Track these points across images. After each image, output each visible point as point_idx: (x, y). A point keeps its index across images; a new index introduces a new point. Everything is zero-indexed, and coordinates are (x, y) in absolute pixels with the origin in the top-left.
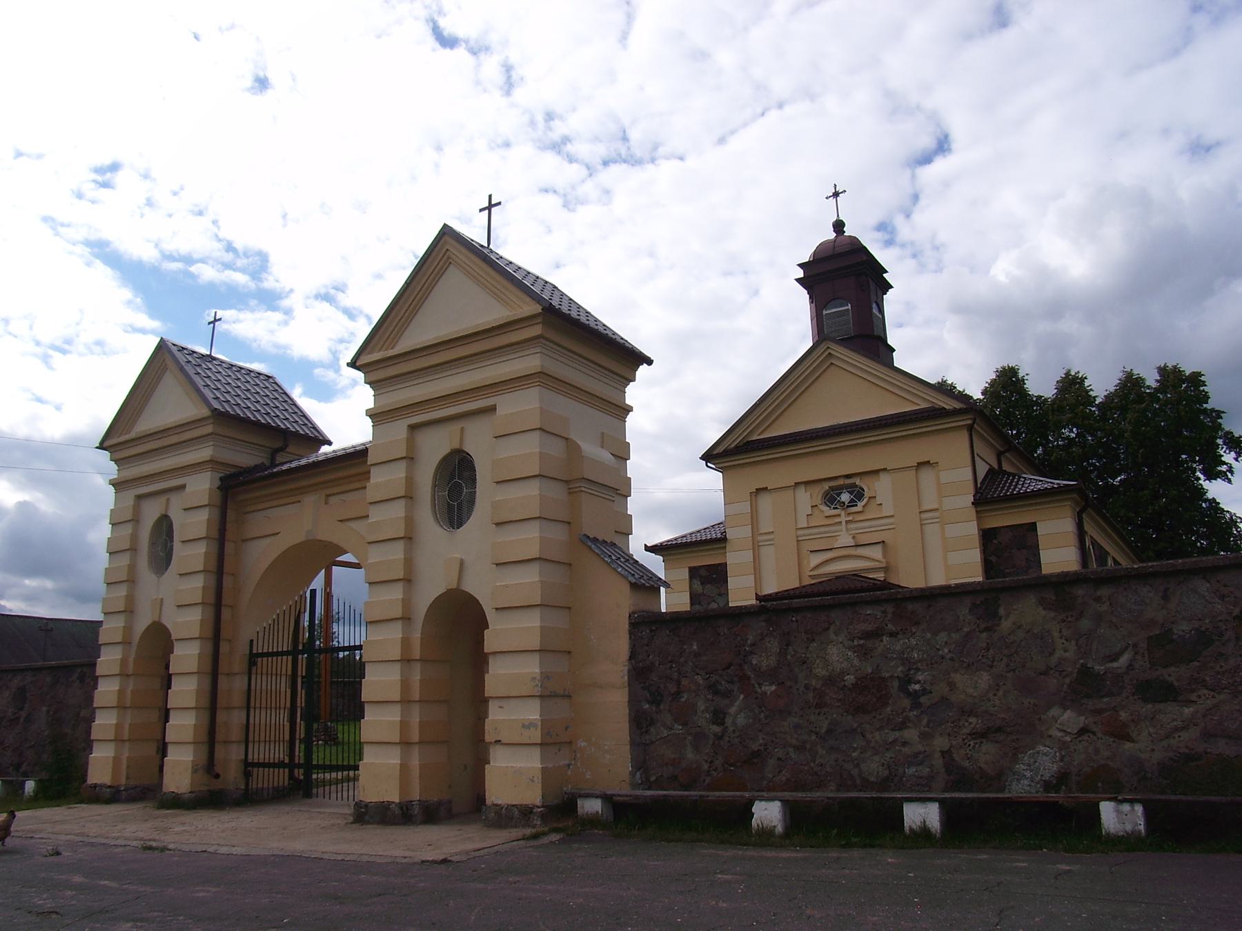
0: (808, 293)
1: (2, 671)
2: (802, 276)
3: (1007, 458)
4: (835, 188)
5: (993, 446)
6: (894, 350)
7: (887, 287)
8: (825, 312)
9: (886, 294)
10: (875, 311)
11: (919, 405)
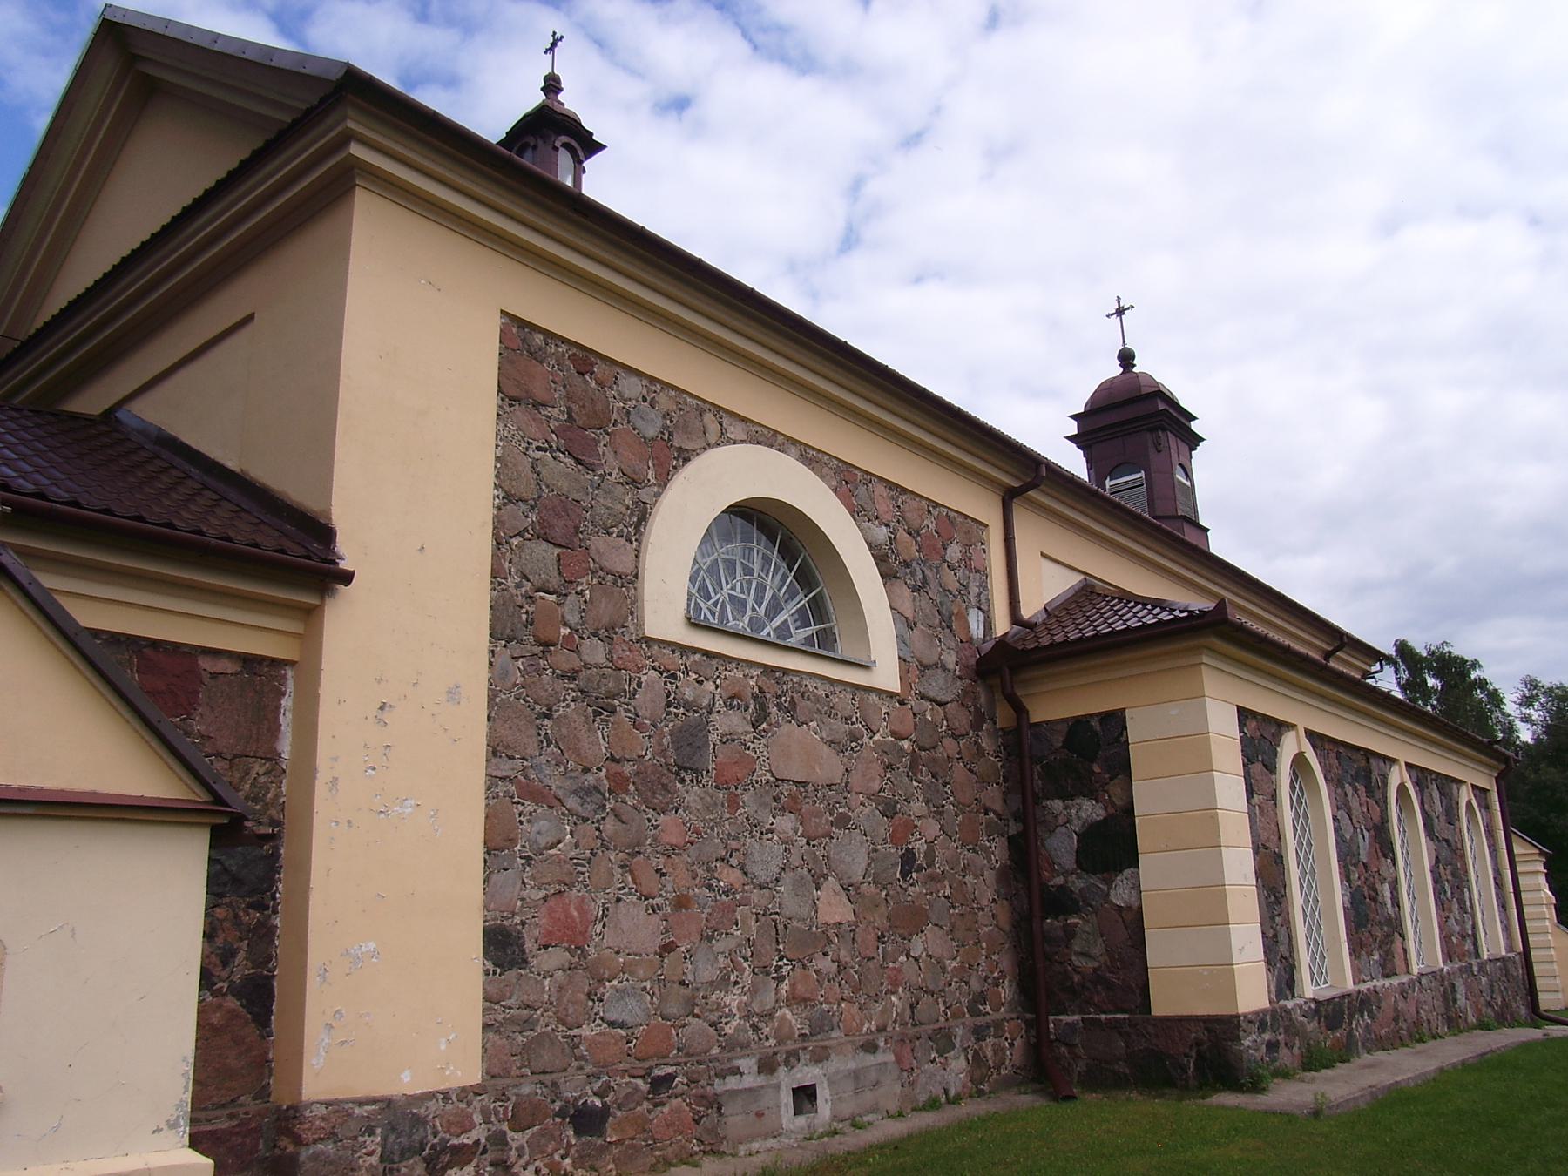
2: (1076, 432)
4: (1119, 302)
6: (1207, 530)
8: (1108, 483)
10: (1180, 477)
11: (200, 797)
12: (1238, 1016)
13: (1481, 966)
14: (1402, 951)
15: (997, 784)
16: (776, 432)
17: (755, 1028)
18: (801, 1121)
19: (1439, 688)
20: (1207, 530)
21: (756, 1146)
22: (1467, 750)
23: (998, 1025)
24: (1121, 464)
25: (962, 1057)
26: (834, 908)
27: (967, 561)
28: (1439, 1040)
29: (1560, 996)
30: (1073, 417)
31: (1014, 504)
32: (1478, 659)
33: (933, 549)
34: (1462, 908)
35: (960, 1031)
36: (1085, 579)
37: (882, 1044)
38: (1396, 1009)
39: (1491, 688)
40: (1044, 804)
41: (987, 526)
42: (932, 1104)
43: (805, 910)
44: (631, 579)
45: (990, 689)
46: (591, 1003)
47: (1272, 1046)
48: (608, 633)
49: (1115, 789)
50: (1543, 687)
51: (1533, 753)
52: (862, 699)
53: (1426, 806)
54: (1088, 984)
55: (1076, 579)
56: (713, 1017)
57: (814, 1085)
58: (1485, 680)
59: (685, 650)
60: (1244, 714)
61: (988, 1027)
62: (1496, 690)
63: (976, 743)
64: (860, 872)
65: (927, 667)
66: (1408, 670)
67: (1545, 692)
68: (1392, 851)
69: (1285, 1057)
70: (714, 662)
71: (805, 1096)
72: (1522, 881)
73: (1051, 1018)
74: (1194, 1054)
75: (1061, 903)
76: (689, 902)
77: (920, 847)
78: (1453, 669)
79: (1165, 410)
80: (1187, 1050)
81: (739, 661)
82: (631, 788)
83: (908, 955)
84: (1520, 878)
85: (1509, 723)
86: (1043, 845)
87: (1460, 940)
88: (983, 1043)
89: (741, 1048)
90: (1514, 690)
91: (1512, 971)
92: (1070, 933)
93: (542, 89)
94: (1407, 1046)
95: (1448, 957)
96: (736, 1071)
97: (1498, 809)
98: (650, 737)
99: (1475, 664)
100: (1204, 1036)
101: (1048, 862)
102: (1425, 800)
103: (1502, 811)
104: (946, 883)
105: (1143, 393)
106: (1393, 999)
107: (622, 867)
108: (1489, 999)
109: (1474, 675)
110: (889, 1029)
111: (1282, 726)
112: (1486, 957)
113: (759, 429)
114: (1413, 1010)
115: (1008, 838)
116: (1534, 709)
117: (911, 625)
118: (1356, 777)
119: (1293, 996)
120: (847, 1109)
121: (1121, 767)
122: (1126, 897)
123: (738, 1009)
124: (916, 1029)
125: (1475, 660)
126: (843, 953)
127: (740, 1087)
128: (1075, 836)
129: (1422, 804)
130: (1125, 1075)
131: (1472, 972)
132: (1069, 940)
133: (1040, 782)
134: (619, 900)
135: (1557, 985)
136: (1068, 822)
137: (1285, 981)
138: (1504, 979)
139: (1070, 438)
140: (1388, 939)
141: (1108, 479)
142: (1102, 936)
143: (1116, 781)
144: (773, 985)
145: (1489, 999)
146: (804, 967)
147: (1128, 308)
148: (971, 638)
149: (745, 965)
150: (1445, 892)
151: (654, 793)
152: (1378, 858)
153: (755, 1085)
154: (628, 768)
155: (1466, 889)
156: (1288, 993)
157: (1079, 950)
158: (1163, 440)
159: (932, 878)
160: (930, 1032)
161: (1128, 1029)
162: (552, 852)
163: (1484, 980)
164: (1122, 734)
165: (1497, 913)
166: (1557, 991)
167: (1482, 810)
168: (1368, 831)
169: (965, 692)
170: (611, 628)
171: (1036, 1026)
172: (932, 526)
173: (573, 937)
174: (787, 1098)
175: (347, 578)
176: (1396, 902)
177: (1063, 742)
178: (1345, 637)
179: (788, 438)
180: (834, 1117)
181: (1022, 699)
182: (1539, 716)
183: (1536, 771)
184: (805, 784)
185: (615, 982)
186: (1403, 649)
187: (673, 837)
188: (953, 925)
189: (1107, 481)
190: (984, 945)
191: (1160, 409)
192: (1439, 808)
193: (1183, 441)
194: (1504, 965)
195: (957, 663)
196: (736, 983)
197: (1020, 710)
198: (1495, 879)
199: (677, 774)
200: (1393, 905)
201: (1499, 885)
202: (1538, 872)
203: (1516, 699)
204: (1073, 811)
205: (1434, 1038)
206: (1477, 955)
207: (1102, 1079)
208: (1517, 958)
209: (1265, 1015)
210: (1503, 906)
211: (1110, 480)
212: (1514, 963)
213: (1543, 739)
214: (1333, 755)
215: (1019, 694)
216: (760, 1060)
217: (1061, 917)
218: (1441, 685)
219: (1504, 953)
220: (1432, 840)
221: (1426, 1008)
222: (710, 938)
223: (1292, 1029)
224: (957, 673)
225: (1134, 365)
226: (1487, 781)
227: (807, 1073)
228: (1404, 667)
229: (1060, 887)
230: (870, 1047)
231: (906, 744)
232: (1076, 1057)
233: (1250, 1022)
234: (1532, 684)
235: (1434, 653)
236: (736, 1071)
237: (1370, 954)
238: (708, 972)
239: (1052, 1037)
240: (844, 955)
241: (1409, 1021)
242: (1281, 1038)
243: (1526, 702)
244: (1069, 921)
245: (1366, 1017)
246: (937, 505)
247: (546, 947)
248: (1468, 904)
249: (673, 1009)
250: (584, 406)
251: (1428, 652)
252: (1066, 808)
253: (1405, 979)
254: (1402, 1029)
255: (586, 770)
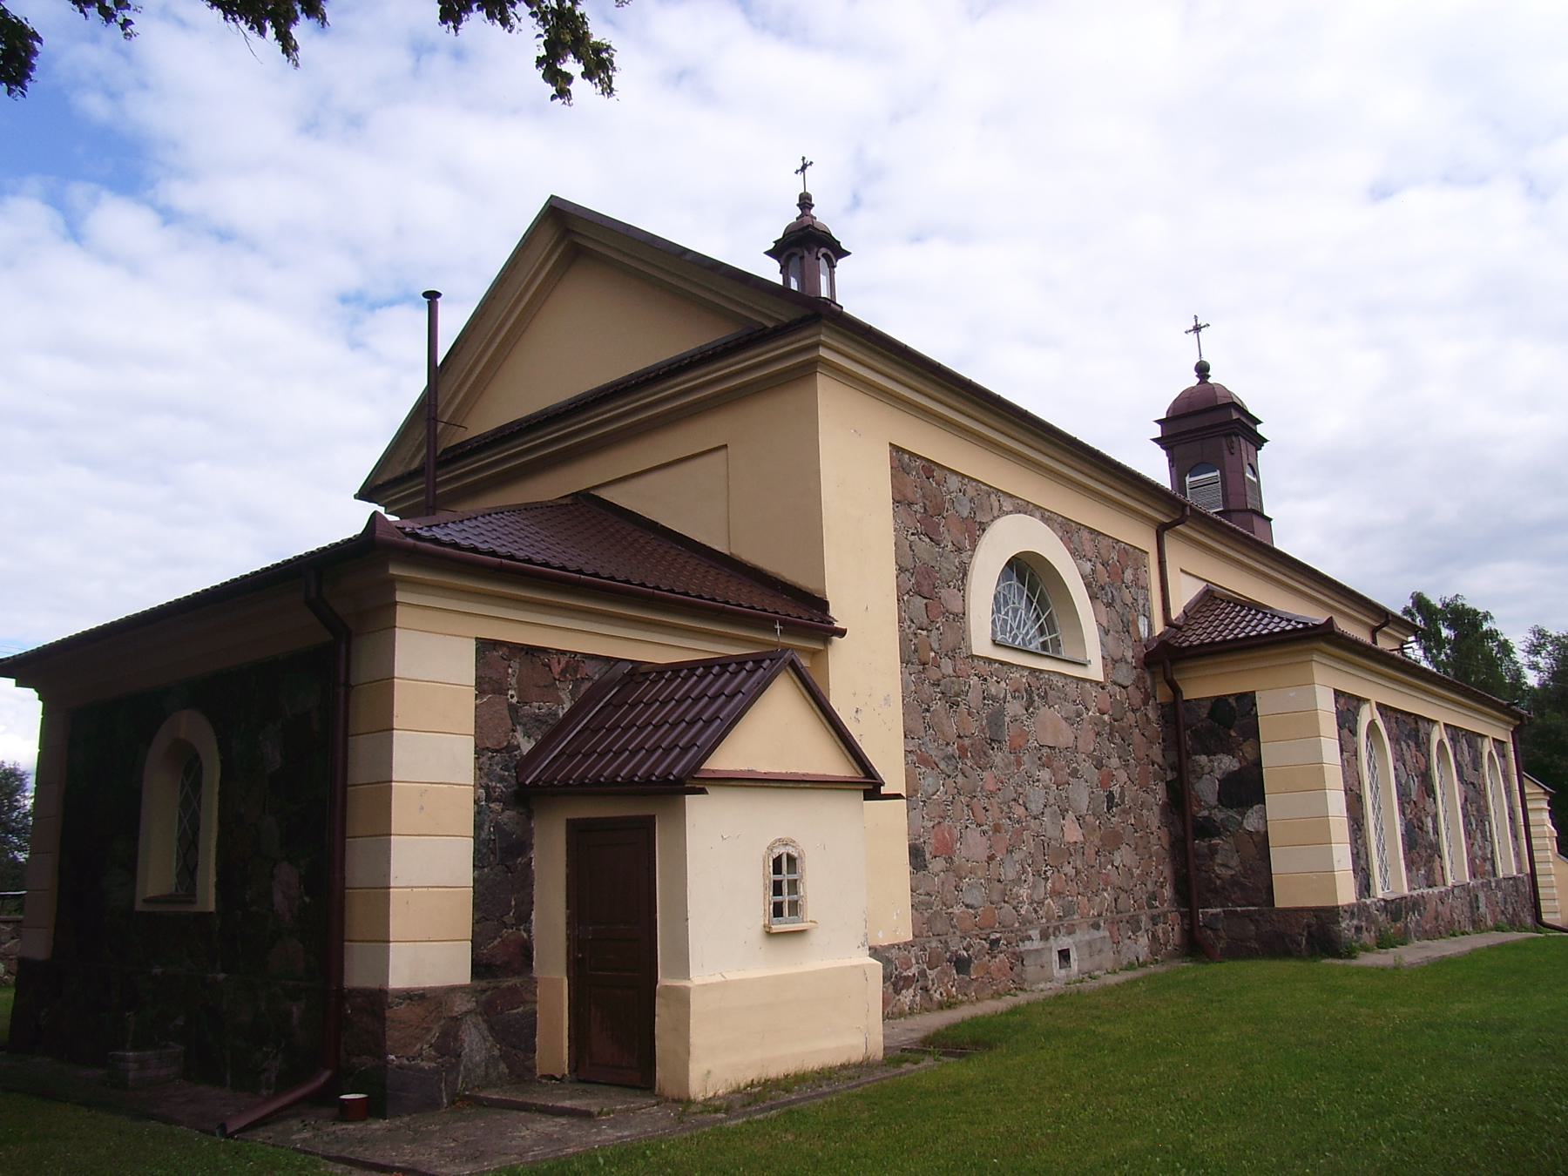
0: (1167, 455)
1: (2, 922)
2: (1160, 435)
3: (1387, 634)
4: (1196, 321)
5: (1365, 624)
7: (1259, 441)
8: (1188, 479)
9: (1260, 449)
10: (1249, 475)
12: (1338, 907)
13: (1498, 883)
14: (1439, 868)
15: (1159, 743)
16: (1028, 502)
17: (1036, 912)
18: (1063, 972)
19: (1453, 638)
20: (1270, 520)
21: (1041, 986)
22: (1488, 710)
23: (1165, 915)
24: (1197, 465)
25: (1146, 936)
26: (1073, 834)
27: (1136, 580)
28: (1467, 936)
29: (1559, 916)
30: (1158, 422)
31: (1165, 535)
32: (1489, 611)
33: (1116, 574)
34: (1484, 837)
35: (1144, 918)
36: (1207, 585)
37: (1102, 924)
38: (1437, 911)
39: (1502, 638)
40: (1193, 758)
41: (1147, 553)
42: (1130, 967)
43: (1057, 834)
44: (962, 616)
45: (1153, 675)
46: (956, 893)
47: (1358, 929)
48: (952, 654)
49: (1247, 748)
50: (1550, 636)
51: (1539, 698)
52: (1082, 688)
53: (1458, 756)
54: (1227, 887)
55: (1201, 586)
56: (1015, 903)
57: (1068, 950)
58: (1496, 631)
59: (990, 661)
60: (1338, 694)
61: (1159, 916)
62: (1507, 641)
63: (1146, 714)
64: (1086, 808)
65: (1116, 662)
66: (1424, 620)
67: (1553, 641)
68: (1434, 792)
69: (1368, 938)
70: (1005, 668)
71: (1064, 955)
72: (1531, 816)
73: (1200, 910)
74: (1305, 933)
75: (1207, 829)
76: (1000, 828)
77: (1116, 789)
78: (1466, 621)
79: (1238, 419)
80: (1301, 931)
81: (1018, 666)
82: (969, 755)
83: (1113, 865)
84: (1530, 814)
85: (1518, 670)
86: (1194, 789)
87: (1482, 863)
88: (1157, 927)
89: (1030, 923)
90: (1524, 639)
91: (1521, 887)
92: (1213, 851)
93: (798, 205)
94: (1444, 938)
95: (1473, 875)
96: (1030, 938)
97: (1513, 757)
98: (976, 721)
99: (1487, 616)
100: (1314, 921)
101: (1196, 800)
102: (1458, 752)
103: (1516, 759)
104: (1132, 815)
105: (1219, 403)
106: (1434, 903)
107: (967, 806)
108: (1503, 908)
109: (1485, 626)
110: (1104, 915)
111: (1361, 701)
112: (1501, 876)
113: (1019, 502)
114: (1449, 913)
115: (1166, 782)
116: (1541, 657)
117: (1107, 633)
118: (1409, 737)
119: (1369, 896)
120: (1087, 966)
121: (1252, 732)
122: (1255, 825)
123: (1027, 898)
124: (1119, 915)
125: (1487, 612)
126: (1078, 862)
127: (1032, 948)
128: (1217, 782)
129: (1455, 755)
130: (1256, 949)
131: (1491, 886)
132: (1213, 855)
133: (1190, 743)
134: (967, 827)
135: (1556, 906)
136: (1212, 771)
137: (1365, 887)
138: (1515, 894)
139: (1155, 440)
140: (1430, 859)
141: (1188, 476)
142: (1238, 852)
143: (1248, 742)
144: (1043, 882)
145: (1503, 908)
146: (1059, 871)
147: (1204, 326)
148: (1141, 638)
149: (1029, 869)
150: (1471, 825)
151: (980, 758)
152: (1424, 798)
153: (1039, 947)
154: (967, 742)
155: (1487, 823)
156: (1366, 894)
157: (1220, 862)
158: (1236, 445)
159: (1124, 811)
160: (1127, 918)
161: (1257, 917)
162: (935, 797)
163: (1499, 894)
164: (1252, 709)
165: (1510, 841)
166: (1556, 912)
167: (1501, 759)
168: (1417, 777)
169: (1138, 678)
170: (953, 650)
171: (1189, 917)
172: (1116, 558)
173: (946, 852)
174: (1055, 957)
175: (842, 633)
176: (1436, 832)
177: (1208, 714)
178: (1390, 616)
179: (1035, 505)
180: (1079, 971)
181: (1178, 682)
182: (1546, 663)
183: (1542, 715)
184: (1054, 748)
185: (967, 880)
186: (1419, 602)
187: (991, 786)
188: (1136, 843)
189: (1187, 478)
190: (1154, 859)
191: (1234, 418)
192: (1467, 758)
193: (1250, 443)
194: (1516, 883)
195: (1133, 657)
196: (1025, 881)
197: (1176, 691)
198: (1509, 814)
199: (990, 745)
200: (1434, 834)
201: (1512, 819)
202: (1542, 809)
203: (1524, 648)
204: (1216, 764)
205: (1463, 934)
206: (1495, 875)
207: (1237, 951)
208: (1525, 878)
209: (1354, 908)
210: (1515, 837)
211: (1190, 477)
212: (1523, 881)
213: (1549, 685)
214: (1393, 720)
215: (1175, 678)
216: (1041, 931)
217: (1206, 839)
218: (1455, 635)
219: (1515, 873)
220: (1462, 783)
221: (1458, 912)
222: (1011, 851)
223: (1370, 919)
224: (1134, 664)
225: (1209, 376)
226: (1505, 735)
227: (1065, 942)
228: (1420, 618)
229: (1204, 817)
230: (1096, 926)
231: (1106, 717)
232: (1219, 938)
233: (1345, 911)
234: (1541, 634)
235: (1448, 605)
236: (1030, 938)
237: (1418, 870)
238: (1012, 875)
239: (1201, 924)
240: (1079, 865)
241: (1446, 920)
242: (1363, 924)
243: (1534, 650)
244: (1212, 842)
245: (1416, 915)
246: (1119, 541)
247: (935, 857)
248: (1488, 833)
249: (995, 898)
250: (931, 501)
251: (1443, 605)
252: (1211, 761)
253: (1443, 889)
254: (1440, 925)
255: (948, 744)
